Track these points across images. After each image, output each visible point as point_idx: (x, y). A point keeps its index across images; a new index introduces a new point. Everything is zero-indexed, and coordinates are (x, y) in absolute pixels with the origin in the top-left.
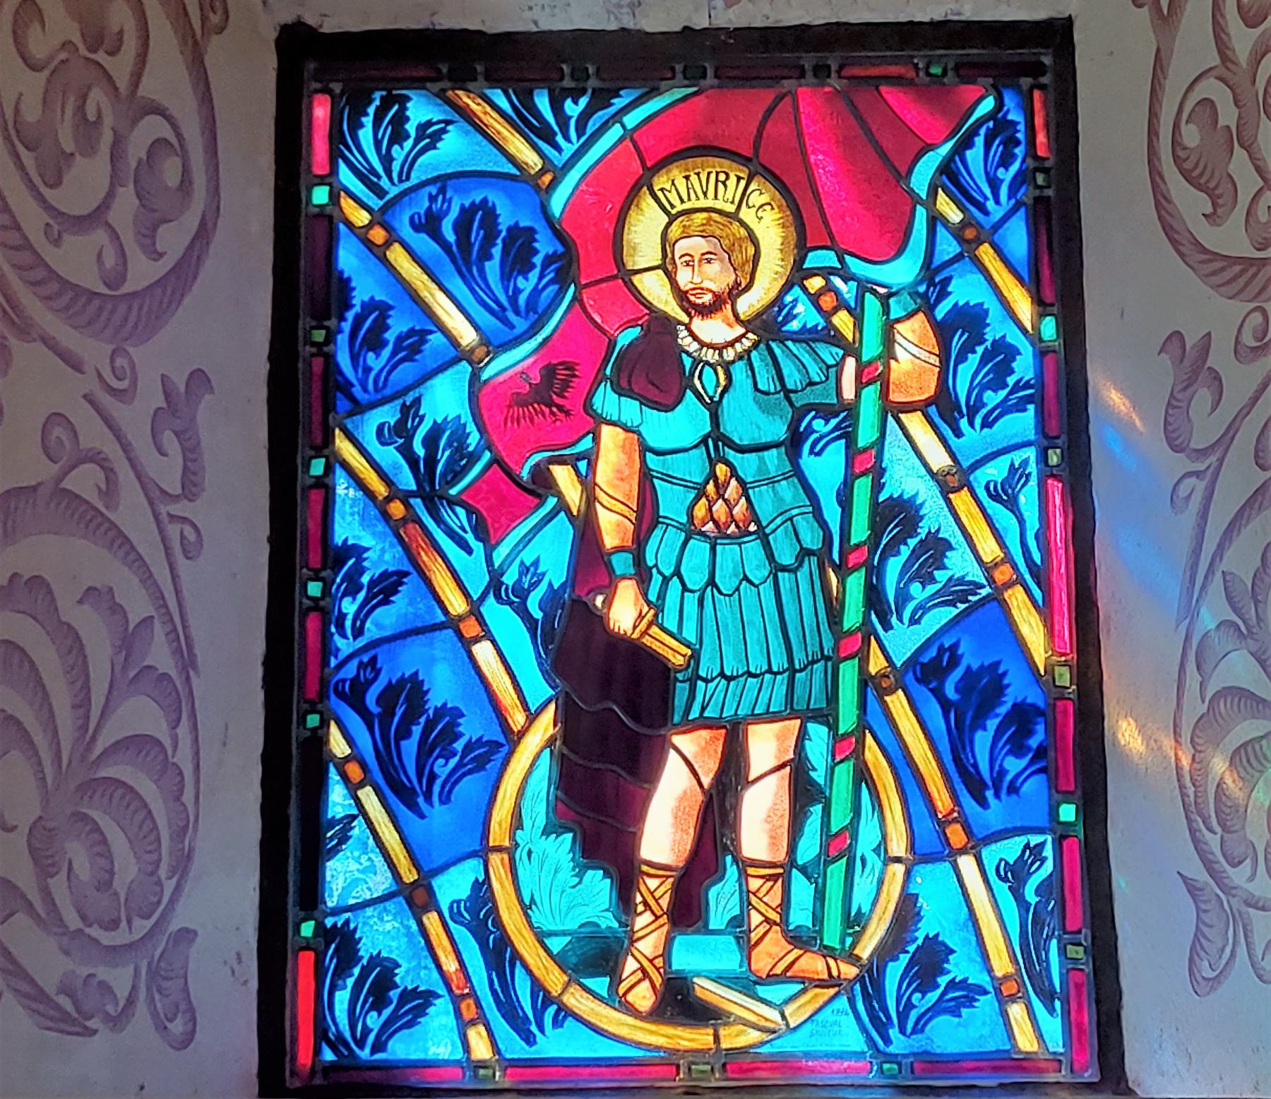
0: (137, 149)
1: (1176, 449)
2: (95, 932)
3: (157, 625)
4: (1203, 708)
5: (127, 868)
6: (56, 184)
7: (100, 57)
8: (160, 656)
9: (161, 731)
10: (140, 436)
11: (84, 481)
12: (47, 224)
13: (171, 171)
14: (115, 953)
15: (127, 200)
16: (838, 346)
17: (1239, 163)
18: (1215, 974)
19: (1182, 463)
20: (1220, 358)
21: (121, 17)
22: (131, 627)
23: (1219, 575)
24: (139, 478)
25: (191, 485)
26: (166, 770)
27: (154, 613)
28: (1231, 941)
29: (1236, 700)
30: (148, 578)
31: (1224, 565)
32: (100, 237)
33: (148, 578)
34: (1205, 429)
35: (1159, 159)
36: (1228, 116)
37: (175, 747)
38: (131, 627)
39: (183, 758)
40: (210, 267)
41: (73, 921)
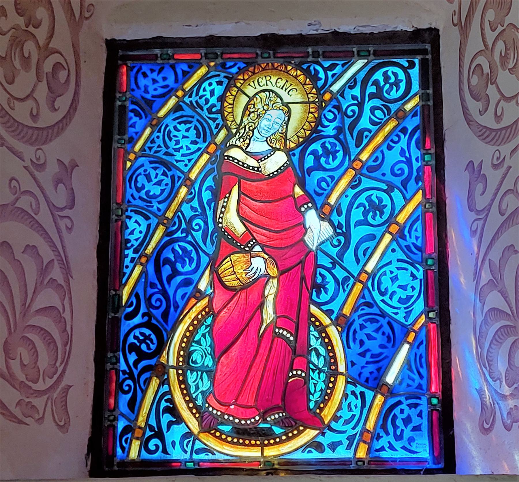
0: (48, 66)
1: (471, 210)
2: (30, 384)
3: (56, 262)
4: (482, 318)
5: (44, 362)
6: (11, 82)
7: (31, 29)
8: (56, 273)
9: (58, 304)
10: (49, 188)
11: (24, 203)
12: (8, 99)
13: (62, 75)
14: (39, 393)
15: (43, 87)
16: (328, 67)
17: (491, 90)
18: (489, 425)
19: (473, 216)
20: (487, 170)
21: (41, 13)
22: (45, 264)
23: (487, 262)
24: (47, 201)
25: (72, 204)
26: (60, 320)
27: (53, 257)
28: (488, 377)
29: (496, 312)
30: (53, 246)
31: (489, 257)
32: (30, 103)
33: (53, 246)
34: (481, 203)
35: (465, 102)
36: (486, 69)
37: (64, 310)
38: (45, 264)
39: (67, 315)
40: (81, 105)
41: (21, 377)
